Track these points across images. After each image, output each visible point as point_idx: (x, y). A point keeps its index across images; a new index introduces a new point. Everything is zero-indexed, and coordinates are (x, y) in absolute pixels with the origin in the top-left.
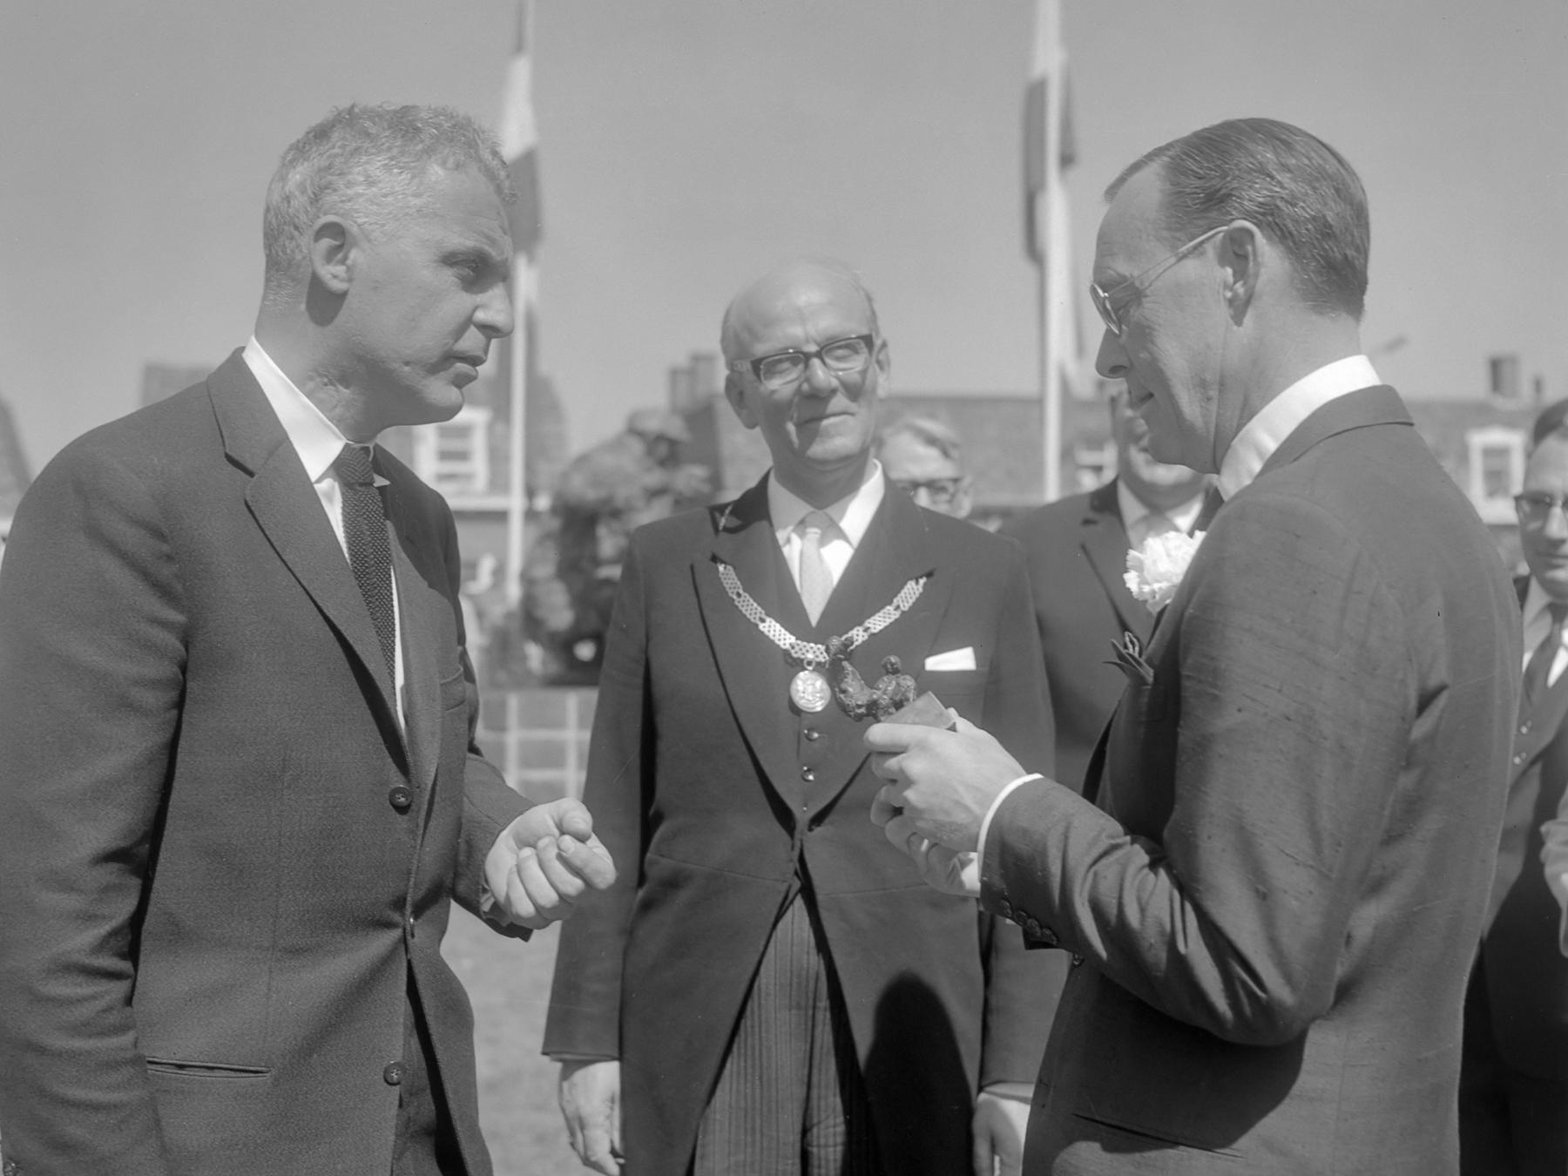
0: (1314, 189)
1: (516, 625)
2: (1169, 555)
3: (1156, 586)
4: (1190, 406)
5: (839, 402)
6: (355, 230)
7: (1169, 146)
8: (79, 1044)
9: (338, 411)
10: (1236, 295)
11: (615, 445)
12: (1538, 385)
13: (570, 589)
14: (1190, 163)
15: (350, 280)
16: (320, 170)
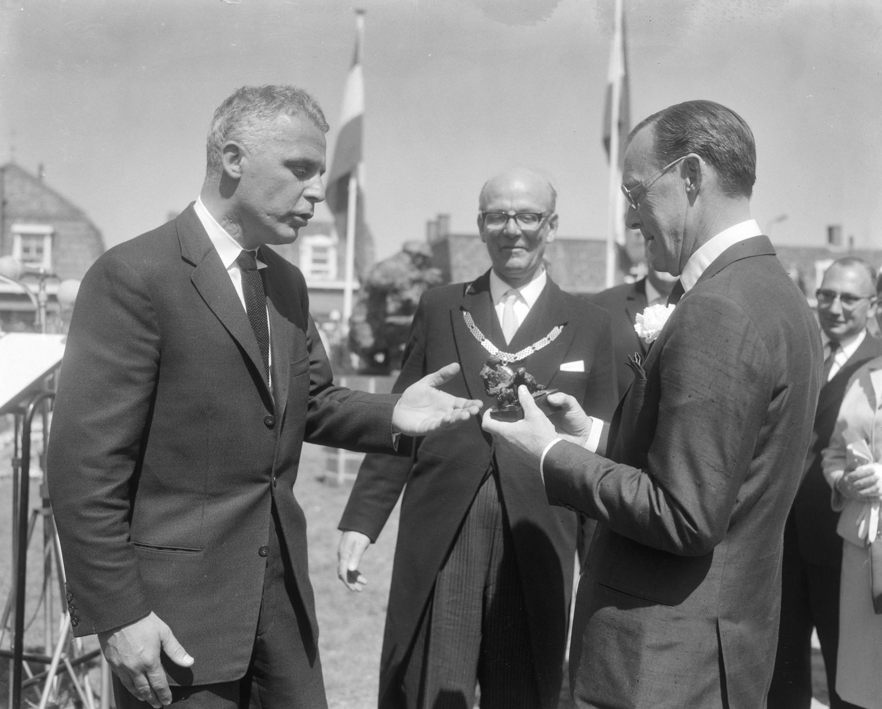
0: (728, 137)
1: (345, 344)
2: (656, 316)
3: (650, 332)
4: (670, 244)
5: (521, 242)
6: (242, 148)
7: (657, 115)
8: (106, 540)
9: (237, 235)
10: (692, 190)
11: (397, 258)
12: (851, 240)
13: (373, 328)
14: (668, 126)
15: (241, 172)
16: (228, 120)
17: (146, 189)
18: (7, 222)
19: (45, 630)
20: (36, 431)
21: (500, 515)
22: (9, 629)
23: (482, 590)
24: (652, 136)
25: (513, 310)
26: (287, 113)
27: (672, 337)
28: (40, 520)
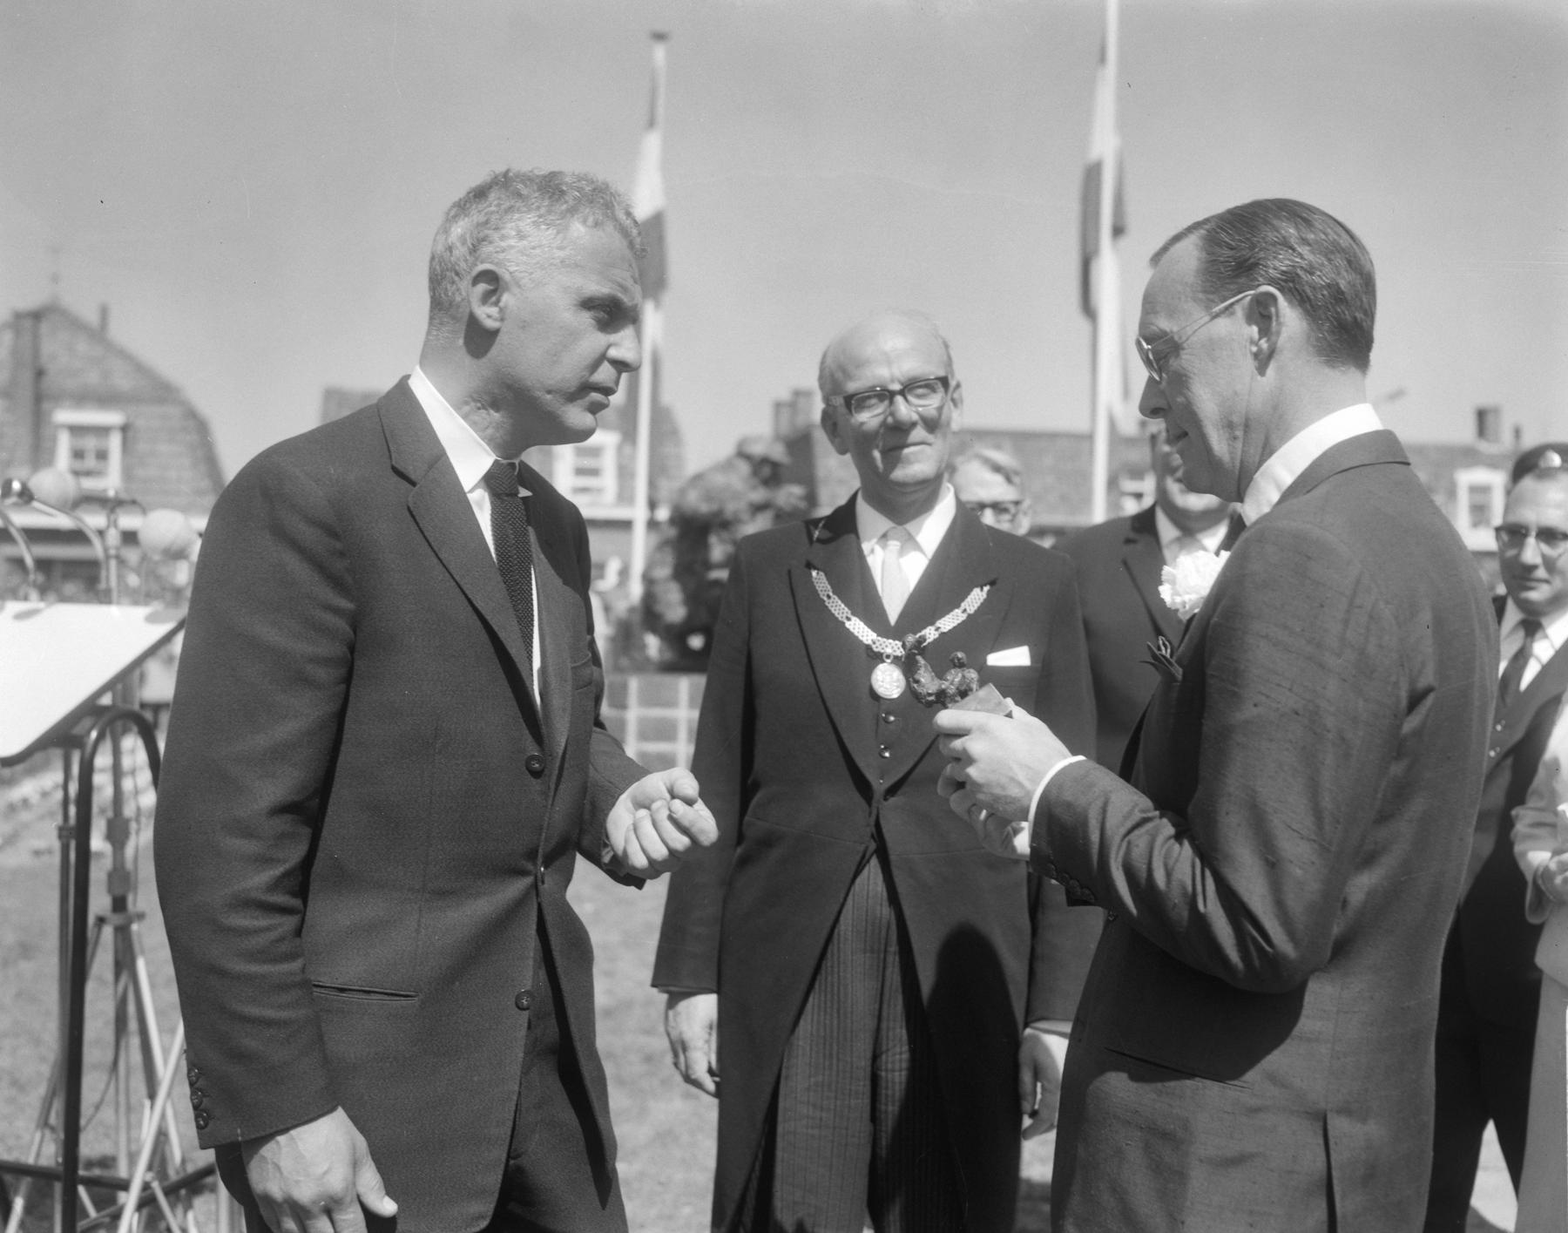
0: (1330, 260)
1: (637, 618)
3: (1187, 598)
4: (1219, 444)
5: (919, 433)
6: (507, 277)
7: (1207, 221)
9: (490, 431)
10: (1260, 350)
11: (726, 466)
12: (1517, 433)
13: (685, 589)
15: (502, 320)
16: (478, 225)
17: (299, 345)
18: (46, 406)
19: (117, 1128)
20: (102, 770)
21: (894, 927)
22: (53, 1129)
23: (869, 1063)
24: (1196, 253)
25: (898, 564)
26: (584, 222)
27: (1223, 603)
28: (108, 932)
